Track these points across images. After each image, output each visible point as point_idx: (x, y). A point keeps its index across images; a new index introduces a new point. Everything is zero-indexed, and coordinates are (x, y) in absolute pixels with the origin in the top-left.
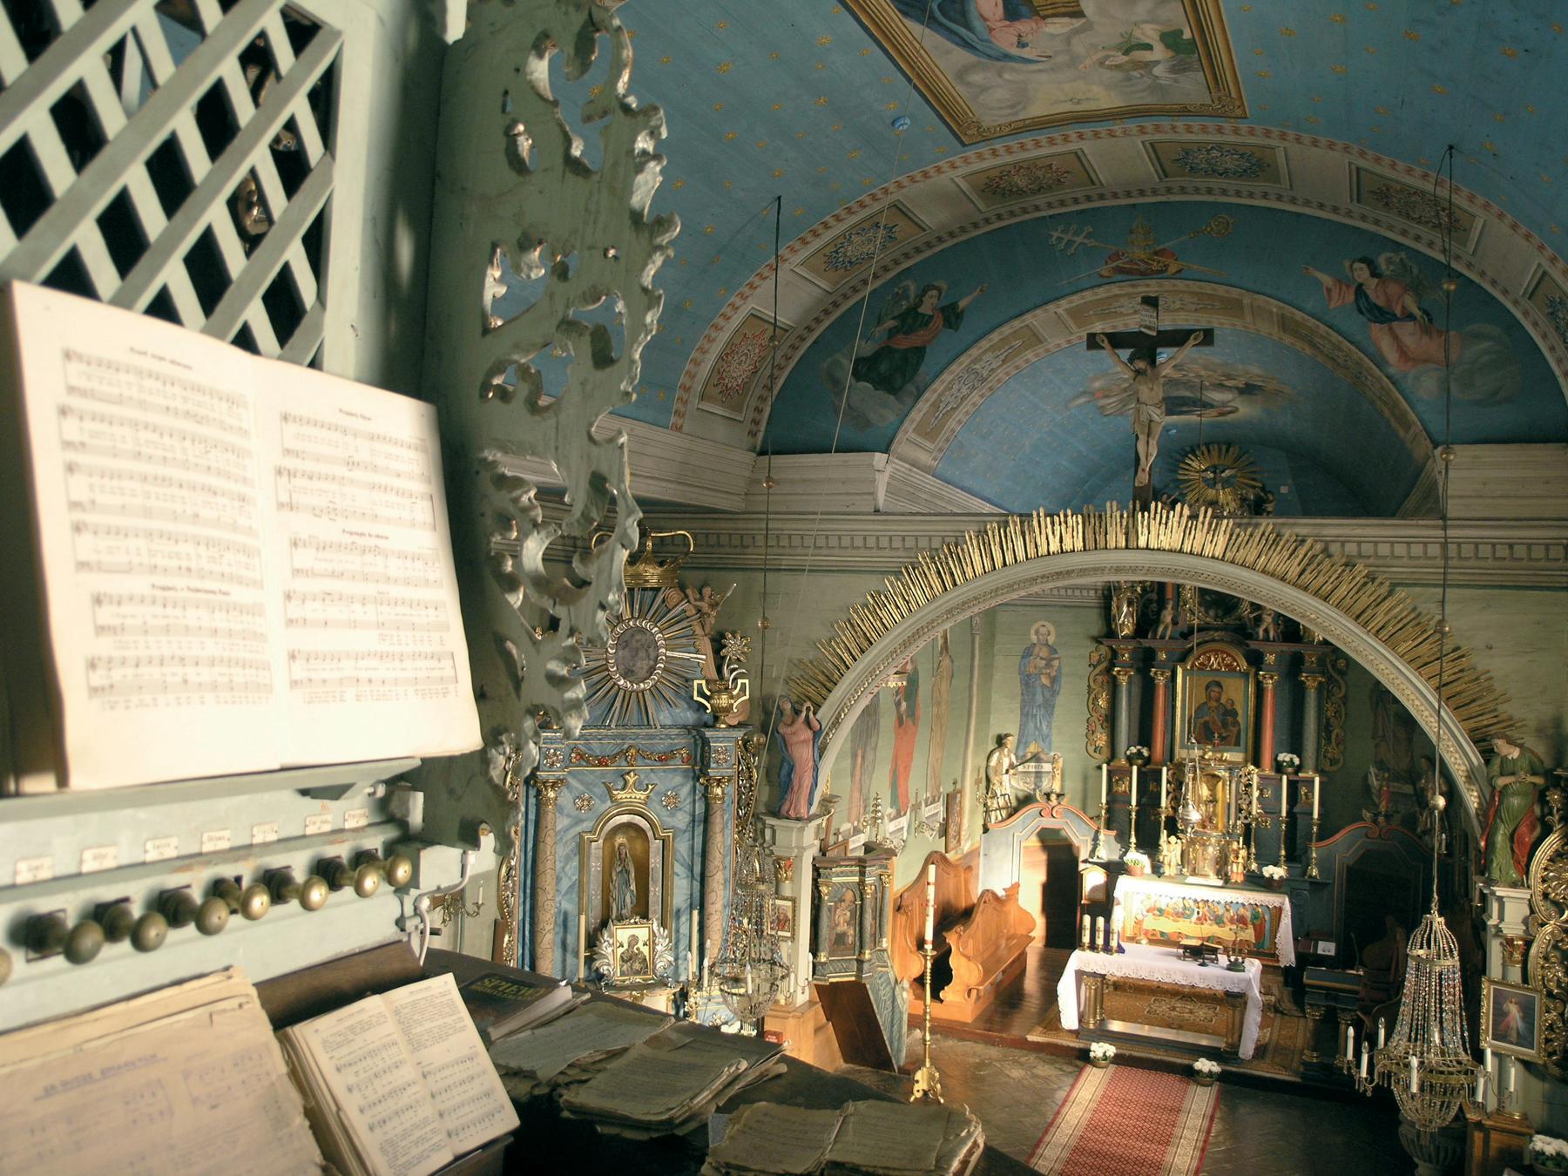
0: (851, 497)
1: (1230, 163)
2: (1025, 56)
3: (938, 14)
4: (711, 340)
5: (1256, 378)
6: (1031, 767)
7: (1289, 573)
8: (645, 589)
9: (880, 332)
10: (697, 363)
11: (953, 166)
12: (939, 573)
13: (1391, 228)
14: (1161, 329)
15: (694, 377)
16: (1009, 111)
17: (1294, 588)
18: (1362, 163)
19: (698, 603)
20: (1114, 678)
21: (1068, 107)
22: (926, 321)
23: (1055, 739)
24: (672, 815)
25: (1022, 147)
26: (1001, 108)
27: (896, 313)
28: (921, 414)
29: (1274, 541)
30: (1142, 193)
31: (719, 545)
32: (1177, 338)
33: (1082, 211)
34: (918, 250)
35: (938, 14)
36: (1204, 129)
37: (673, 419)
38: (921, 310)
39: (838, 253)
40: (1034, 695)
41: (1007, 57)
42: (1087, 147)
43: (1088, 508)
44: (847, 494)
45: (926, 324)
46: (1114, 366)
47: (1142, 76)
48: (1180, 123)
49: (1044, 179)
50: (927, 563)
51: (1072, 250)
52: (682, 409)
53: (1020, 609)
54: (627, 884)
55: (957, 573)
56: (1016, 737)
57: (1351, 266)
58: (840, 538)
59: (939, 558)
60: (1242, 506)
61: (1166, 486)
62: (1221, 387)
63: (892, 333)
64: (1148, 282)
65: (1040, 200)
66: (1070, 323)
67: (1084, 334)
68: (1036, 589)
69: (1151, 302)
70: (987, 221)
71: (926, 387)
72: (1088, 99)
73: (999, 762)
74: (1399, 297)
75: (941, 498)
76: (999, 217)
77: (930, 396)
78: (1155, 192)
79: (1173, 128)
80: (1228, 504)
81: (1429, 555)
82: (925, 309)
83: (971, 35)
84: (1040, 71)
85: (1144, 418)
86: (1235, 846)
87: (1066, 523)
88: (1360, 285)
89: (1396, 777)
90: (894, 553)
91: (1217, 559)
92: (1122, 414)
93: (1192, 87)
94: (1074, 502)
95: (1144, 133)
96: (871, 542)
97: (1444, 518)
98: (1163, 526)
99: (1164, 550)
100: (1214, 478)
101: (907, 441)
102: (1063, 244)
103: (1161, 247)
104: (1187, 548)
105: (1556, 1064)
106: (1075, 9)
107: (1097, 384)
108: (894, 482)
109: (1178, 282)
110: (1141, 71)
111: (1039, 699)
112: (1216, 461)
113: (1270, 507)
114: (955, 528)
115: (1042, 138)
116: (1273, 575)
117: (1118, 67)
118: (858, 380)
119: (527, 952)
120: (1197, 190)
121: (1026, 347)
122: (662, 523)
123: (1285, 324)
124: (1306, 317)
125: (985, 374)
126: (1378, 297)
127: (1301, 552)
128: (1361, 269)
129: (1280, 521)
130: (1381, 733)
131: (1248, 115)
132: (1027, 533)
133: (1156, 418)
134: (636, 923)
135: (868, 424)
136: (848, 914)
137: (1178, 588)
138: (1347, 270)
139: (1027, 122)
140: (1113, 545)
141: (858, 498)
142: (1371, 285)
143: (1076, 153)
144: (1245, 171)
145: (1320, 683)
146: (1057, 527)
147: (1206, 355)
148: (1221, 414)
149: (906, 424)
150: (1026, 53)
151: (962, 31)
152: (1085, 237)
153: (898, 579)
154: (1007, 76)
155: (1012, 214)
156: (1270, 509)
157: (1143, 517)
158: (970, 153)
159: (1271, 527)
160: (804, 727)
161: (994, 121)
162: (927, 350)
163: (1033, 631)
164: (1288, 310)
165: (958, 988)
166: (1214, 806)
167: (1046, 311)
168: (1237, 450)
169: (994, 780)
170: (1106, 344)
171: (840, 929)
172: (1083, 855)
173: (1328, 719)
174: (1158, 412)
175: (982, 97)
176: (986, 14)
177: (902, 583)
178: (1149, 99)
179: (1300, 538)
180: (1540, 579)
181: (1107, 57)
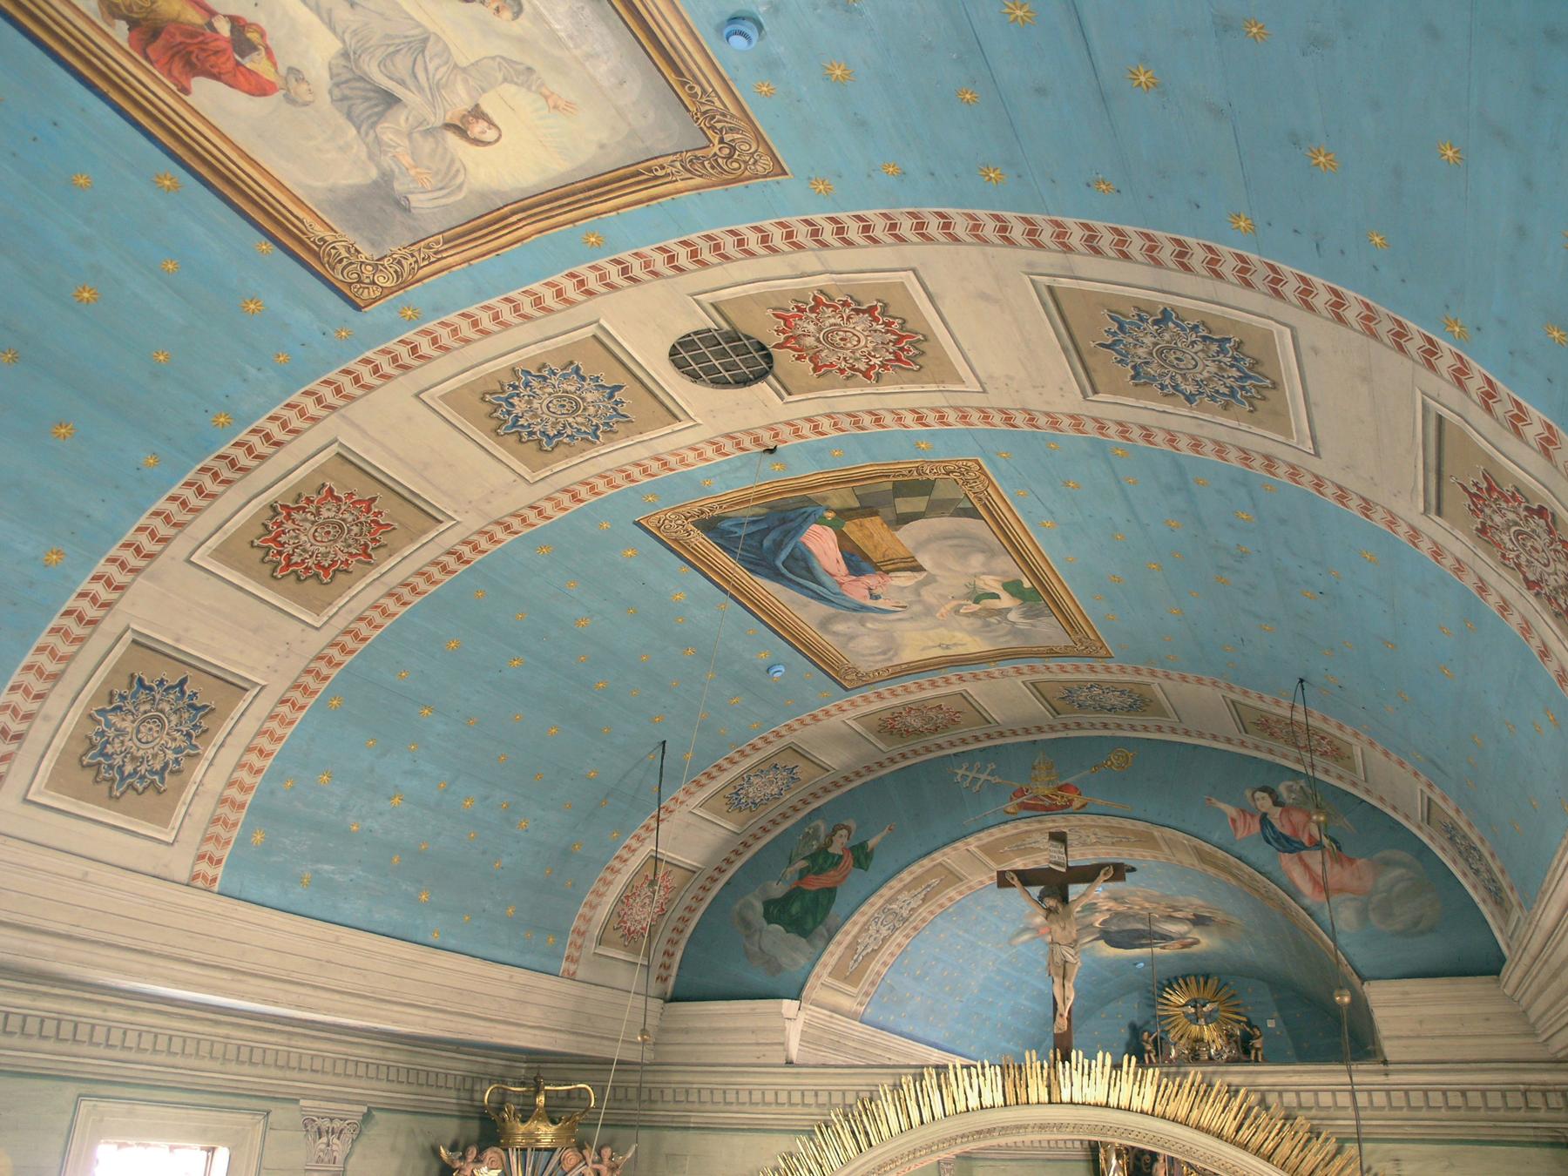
0: (760, 1048)
1: (1113, 699)
3: (784, 571)
4: (607, 883)
7: (1226, 1128)
8: (539, 1150)
10: (593, 907)
12: (853, 1132)
13: (1285, 756)
14: (1070, 865)
15: (590, 920)
17: (1232, 1146)
21: (939, 652)
25: (947, 681)
26: (873, 655)
27: (807, 854)
29: (1205, 1091)
30: (1040, 729)
32: (1088, 874)
34: (826, 790)
35: (784, 571)
36: (1077, 669)
37: (564, 965)
38: (831, 850)
41: (864, 608)
42: (970, 688)
44: (758, 1044)
45: (837, 864)
46: (1022, 904)
47: (1000, 622)
48: (1052, 664)
49: (941, 720)
50: (839, 1121)
52: (576, 954)
53: (999, 1163)
57: (1253, 795)
58: (750, 1093)
59: (853, 1115)
60: (1229, 1043)
61: (1147, 1023)
62: (1170, 918)
63: (803, 874)
64: (1053, 817)
65: (940, 739)
66: (987, 859)
67: (995, 874)
69: (1059, 838)
70: (892, 760)
72: (955, 644)
74: (1305, 827)
75: (875, 1045)
76: (904, 756)
77: (843, 938)
78: (1052, 728)
79: (906, 689)
81: (1375, 1105)
82: (836, 849)
83: (821, 588)
84: (900, 620)
85: (1057, 959)
87: (984, 1075)
90: (806, 1110)
91: (1147, 1114)
93: (1048, 631)
96: (783, 1097)
97: (1385, 1062)
98: (1086, 1077)
99: (1090, 1104)
100: (1196, 1013)
101: (821, 984)
103: (1064, 782)
108: (810, 1031)
109: (1082, 817)
114: (869, 1081)
117: (973, 614)
118: (769, 922)
120: (1093, 726)
122: (570, 1075)
123: (1201, 856)
126: (1283, 826)
128: (1263, 798)
133: (1070, 958)
135: (779, 968)
138: (1250, 800)
139: (903, 666)
140: (1035, 1100)
141: (767, 1048)
142: (1275, 814)
144: (1130, 706)
148: (1184, 946)
149: (817, 969)
150: (880, 604)
151: (814, 586)
152: (989, 775)
154: (869, 625)
156: (1258, 1046)
157: (1064, 1067)
158: (855, 697)
159: (1199, 1077)
162: (839, 891)
168: (1216, 982)
170: (1016, 881)
175: (851, 645)
179: (1233, 1088)
180: (1503, 1132)
181: (961, 606)
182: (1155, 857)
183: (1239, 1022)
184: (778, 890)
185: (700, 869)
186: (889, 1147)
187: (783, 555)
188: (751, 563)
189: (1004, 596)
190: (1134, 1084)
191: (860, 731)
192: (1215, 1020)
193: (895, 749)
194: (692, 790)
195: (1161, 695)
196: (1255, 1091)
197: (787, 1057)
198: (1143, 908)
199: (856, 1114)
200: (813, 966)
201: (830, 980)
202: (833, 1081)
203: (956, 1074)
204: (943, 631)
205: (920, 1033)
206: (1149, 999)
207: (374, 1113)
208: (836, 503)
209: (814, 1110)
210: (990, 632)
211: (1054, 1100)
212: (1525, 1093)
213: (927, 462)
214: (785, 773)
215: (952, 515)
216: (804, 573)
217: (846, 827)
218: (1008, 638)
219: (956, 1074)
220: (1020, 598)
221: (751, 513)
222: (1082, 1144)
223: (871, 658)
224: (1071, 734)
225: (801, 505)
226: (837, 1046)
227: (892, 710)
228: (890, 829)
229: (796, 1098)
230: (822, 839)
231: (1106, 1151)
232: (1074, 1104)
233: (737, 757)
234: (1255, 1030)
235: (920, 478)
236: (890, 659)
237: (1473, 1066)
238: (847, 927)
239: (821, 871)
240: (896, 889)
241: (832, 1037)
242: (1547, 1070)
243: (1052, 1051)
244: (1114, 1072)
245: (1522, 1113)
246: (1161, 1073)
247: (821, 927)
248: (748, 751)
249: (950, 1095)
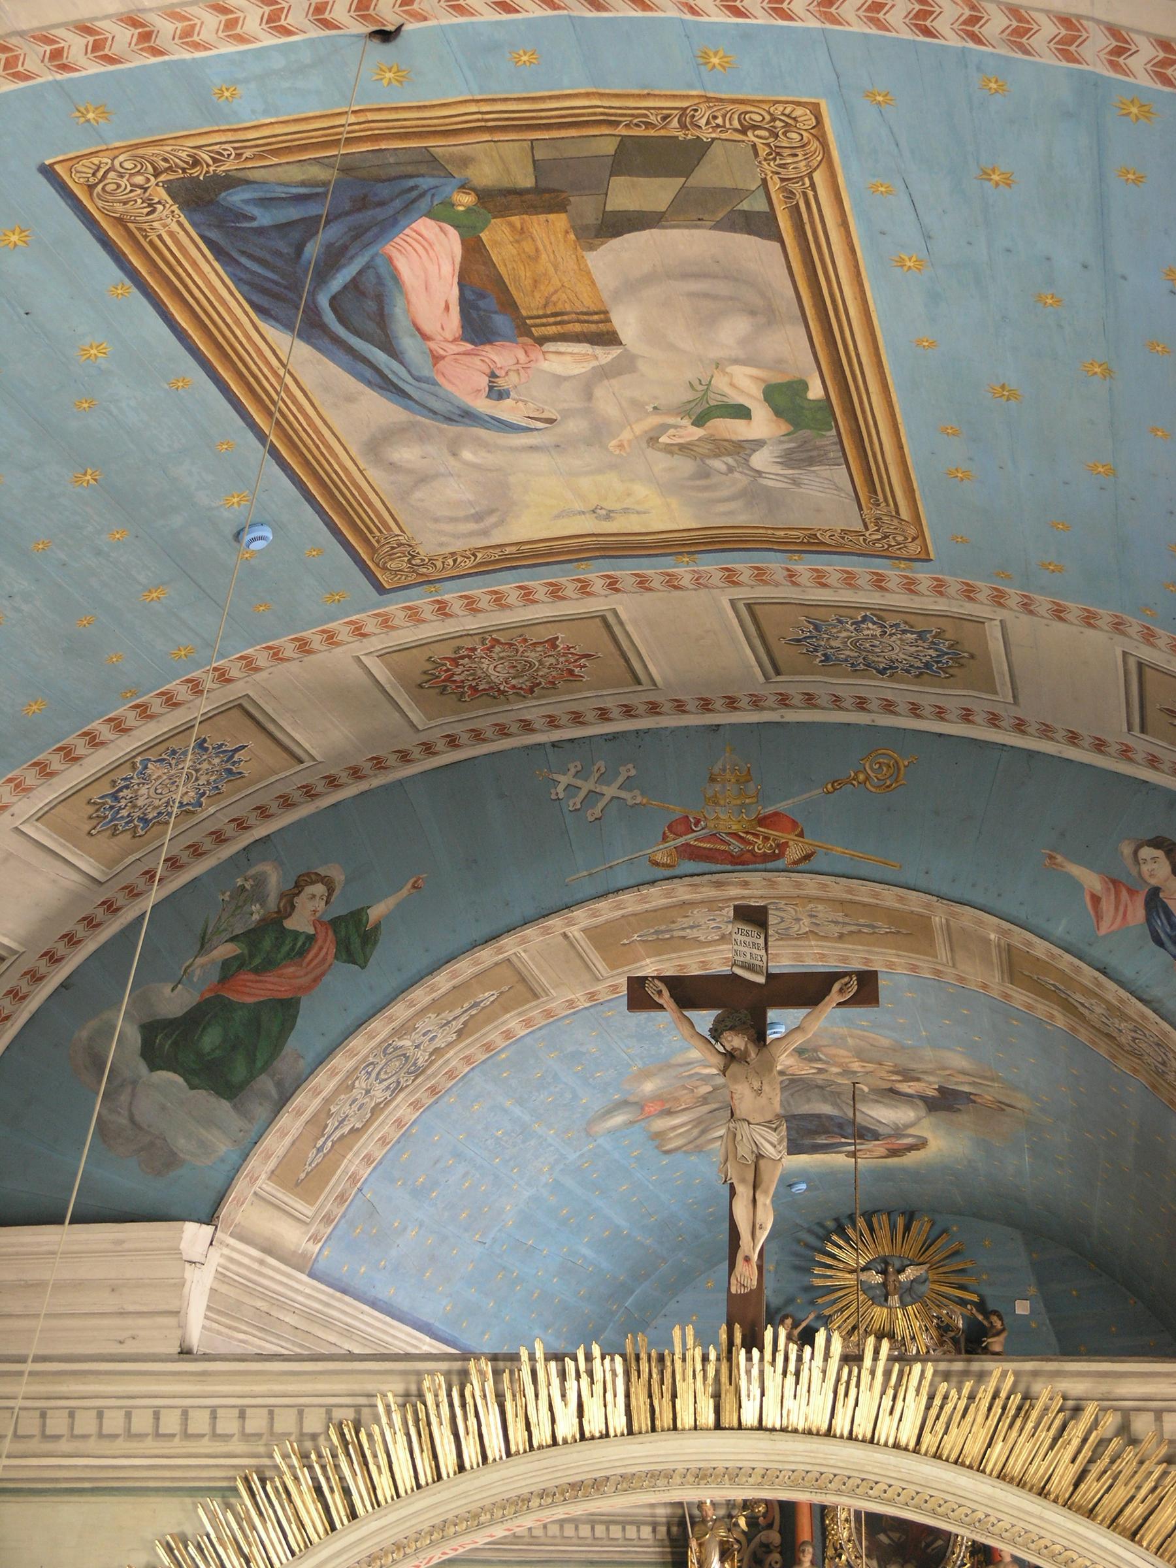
0: (129, 1322)
1: (899, 649)
2: (504, 417)
3: (330, 318)
5: (962, 1078)
7: (1055, 1479)
11: (359, 632)
12: (318, 1490)
14: (772, 971)
16: (472, 526)
17: (1065, 1511)
18: (1146, 653)
21: (587, 525)
22: (302, 946)
25: (499, 600)
26: (453, 520)
28: (288, 1140)
29: (1019, 1409)
30: (732, 703)
33: (614, 737)
34: (287, 803)
35: (330, 318)
36: (849, 580)
38: (289, 924)
39: (117, 799)
41: (467, 416)
43: (635, 1343)
44: (122, 1314)
45: (302, 953)
47: (731, 470)
48: (803, 567)
50: (291, 1467)
51: (597, 811)
55: (358, 1487)
57: (1136, 853)
58: (100, 1415)
59: (320, 1456)
60: (941, 1343)
61: (790, 1301)
62: (892, 1094)
63: (229, 970)
64: (746, 876)
65: (533, 710)
66: (595, 957)
67: (623, 981)
68: (527, 1522)
70: (428, 749)
71: (299, 1082)
72: (626, 511)
75: (327, 1323)
76: (453, 742)
77: (306, 1102)
78: (756, 703)
79: (791, 575)
80: (913, 1338)
83: (395, 365)
84: (532, 448)
85: (744, 1150)
87: (590, 1374)
91: (906, 1449)
92: (699, 1150)
94: (608, 1334)
95: (735, 583)
98: (790, 1379)
99: (796, 1431)
100: (884, 1284)
102: (578, 799)
103: (770, 810)
104: (841, 1425)
106: (602, 327)
107: (649, 1087)
108: (224, 1289)
110: (730, 460)
112: (886, 1250)
113: (996, 1344)
114: (356, 1387)
115: (538, 586)
116: (1021, 1484)
117: (684, 449)
118: (153, 1067)
120: (837, 701)
121: (505, 1005)
124: (1057, 951)
125: (422, 1057)
127: (1076, 1431)
129: (1029, 1366)
131: (932, 557)
132: (508, 1396)
133: (769, 1150)
135: (172, 1160)
137: (823, 1512)
138: (1129, 861)
139: (508, 550)
141: (142, 1322)
143: (604, 619)
144: (927, 665)
146: (571, 1384)
147: (863, 1028)
148: (894, 1153)
149: (253, 1162)
150: (505, 410)
151: (379, 357)
153: (228, 1506)
154: (467, 455)
155: (478, 736)
156: (997, 1348)
157: (749, 1359)
158: (394, 608)
159: (1010, 1380)
161: (441, 545)
162: (304, 1004)
164: (1019, 937)
167: (547, 931)
168: (927, 1227)
170: (666, 999)
174: (774, 1137)
175: (418, 495)
176: (427, 328)
177: (236, 1515)
178: (741, 517)
179: (1070, 1403)
181: (664, 428)
182: (914, 968)
183: (963, 1302)
185: (12, 951)
186: (392, 1517)
187: (338, 282)
188: (264, 291)
189: (762, 414)
190: (883, 1393)
192: (918, 1298)
193: (435, 727)
194: (29, 782)
195: (996, 646)
196: (1116, 1409)
197: (183, 1340)
198: (847, 1072)
199: (326, 1452)
200: (245, 1157)
201: (270, 1187)
202: (277, 1388)
203: (534, 1373)
204: (612, 480)
205: (403, 1302)
206: (796, 1254)
208: (486, 174)
209: (236, 1446)
210: (706, 488)
211: (725, 1423)
213: (708, 99)
214: (216, 761)
215: (718, 226)
216: (371, 327)
218: (732, 506)
219: (534, 1373)
220: (790, 421)
221: (300, 177)
222: (654, 1531)
223: (449, 528)
224: (791, 716)
225: (410, 169)
226: (265, 1323)
227: (458, 642)
228: (414, 887)
230: (272, 902)
231: (700, 1545)
232: (767, 1429)
233: (131, 718)
234: (994, 1319)
235: (681, 135)
236: (485, 533)
239: (268, 965)
240: (419, 1007)
241: (259, 1304)
243: (724, 1327)
244: (846, 1370)
246: (935, 1373)
247: (263, 1077)
248: (156, 706)
249: (521, 1413)
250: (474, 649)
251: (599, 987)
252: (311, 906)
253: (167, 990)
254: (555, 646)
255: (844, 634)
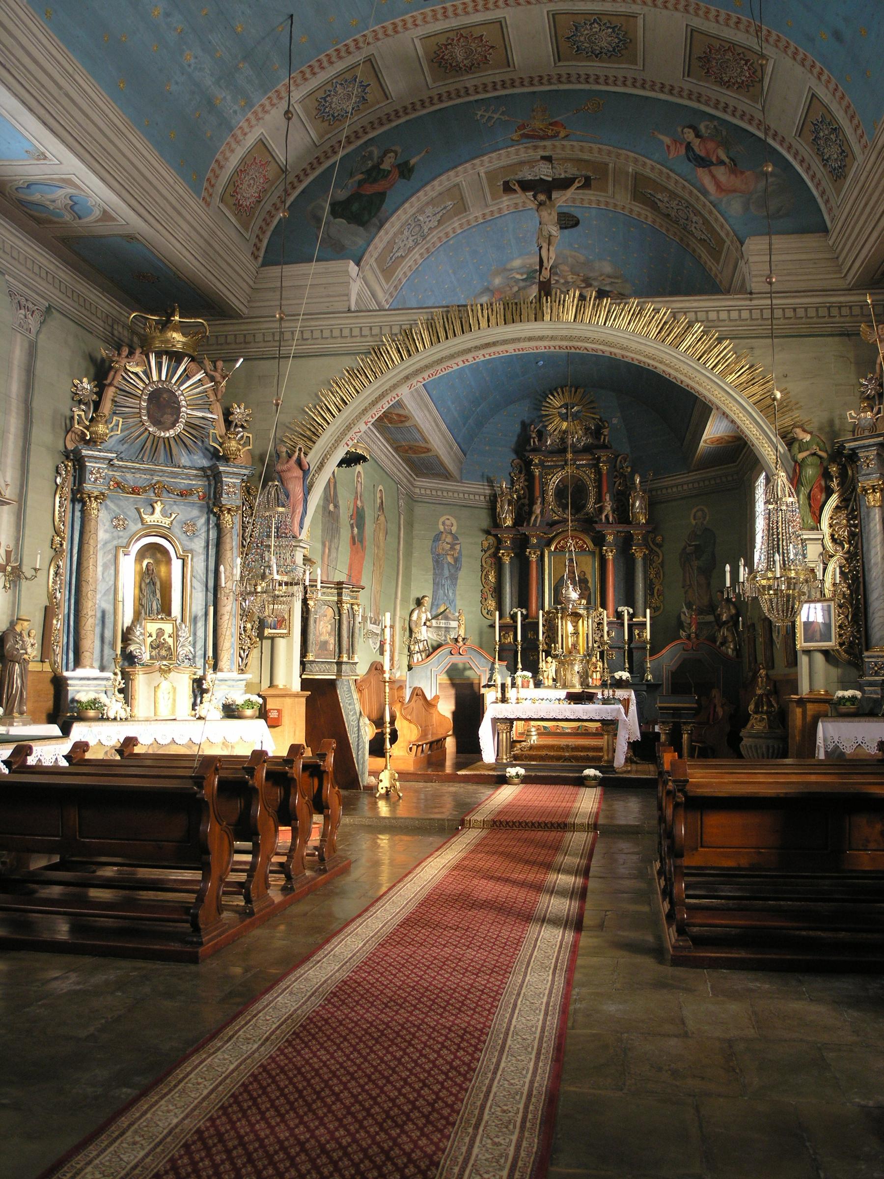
6: (443, 623)
9: (352, 182)
19: (212, 373)
20: (500, 558)
22: (386, 174)
23: (459, 603)
24: (191, 539)
31: (227, 343)
38: (382, 167)
40: (443, 570)
45: (387, 176)
54: (154, 593)
56: (431, 596)
58: (322, 331)
60: (586, 434)
63: (360, 183)
71: (387, 219)
73: (419, 618)
82: (386, 166)
85: (545, 233)
86: (594, 660)
88: (689, 143)
89: (700, 612)
90: (364, 339)
96: (346, 332)
97: (751, 293)
100: (567, 413)
103: (554, 120)
105: (846, 652)
111: (446, 573)
112: (568, 401)
114: (410, 318)
118: (335, 218)
119: (71, 639)
130: (688, 583)
133: (554, 233)
134: (162, 619)
136: (330, 626)
142: (696, 142)
145: (645, 554)
146: (485, 312)
160: (295, 466)
163: (440, 523)
165: (402, 745)
166: (577, 637)
169: (415, 630)
170: (517, 187)
171: (323, 638)
172: (484, 682)
173: (651, 580)
184: (342, 195)
191: (420, 55)
192: (579, 418)
200: (368, 245)
206: (535, 404)
207: (53, 310)
212: (829, 308)
217: (392, 151)
229: (356, 332)
237: (802, 294)
238: (394, 218)
239: (375, 181)
242: (844, 295)
245: (826, 319)
250: (453, 40)
251: (487, 211)
252: (389, 161)
253: (339, 191)
254: (482, 40)
255: (586, 32)
